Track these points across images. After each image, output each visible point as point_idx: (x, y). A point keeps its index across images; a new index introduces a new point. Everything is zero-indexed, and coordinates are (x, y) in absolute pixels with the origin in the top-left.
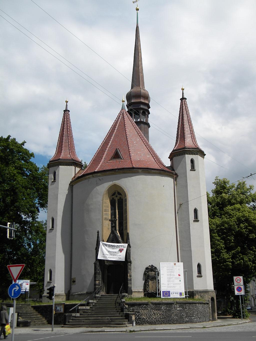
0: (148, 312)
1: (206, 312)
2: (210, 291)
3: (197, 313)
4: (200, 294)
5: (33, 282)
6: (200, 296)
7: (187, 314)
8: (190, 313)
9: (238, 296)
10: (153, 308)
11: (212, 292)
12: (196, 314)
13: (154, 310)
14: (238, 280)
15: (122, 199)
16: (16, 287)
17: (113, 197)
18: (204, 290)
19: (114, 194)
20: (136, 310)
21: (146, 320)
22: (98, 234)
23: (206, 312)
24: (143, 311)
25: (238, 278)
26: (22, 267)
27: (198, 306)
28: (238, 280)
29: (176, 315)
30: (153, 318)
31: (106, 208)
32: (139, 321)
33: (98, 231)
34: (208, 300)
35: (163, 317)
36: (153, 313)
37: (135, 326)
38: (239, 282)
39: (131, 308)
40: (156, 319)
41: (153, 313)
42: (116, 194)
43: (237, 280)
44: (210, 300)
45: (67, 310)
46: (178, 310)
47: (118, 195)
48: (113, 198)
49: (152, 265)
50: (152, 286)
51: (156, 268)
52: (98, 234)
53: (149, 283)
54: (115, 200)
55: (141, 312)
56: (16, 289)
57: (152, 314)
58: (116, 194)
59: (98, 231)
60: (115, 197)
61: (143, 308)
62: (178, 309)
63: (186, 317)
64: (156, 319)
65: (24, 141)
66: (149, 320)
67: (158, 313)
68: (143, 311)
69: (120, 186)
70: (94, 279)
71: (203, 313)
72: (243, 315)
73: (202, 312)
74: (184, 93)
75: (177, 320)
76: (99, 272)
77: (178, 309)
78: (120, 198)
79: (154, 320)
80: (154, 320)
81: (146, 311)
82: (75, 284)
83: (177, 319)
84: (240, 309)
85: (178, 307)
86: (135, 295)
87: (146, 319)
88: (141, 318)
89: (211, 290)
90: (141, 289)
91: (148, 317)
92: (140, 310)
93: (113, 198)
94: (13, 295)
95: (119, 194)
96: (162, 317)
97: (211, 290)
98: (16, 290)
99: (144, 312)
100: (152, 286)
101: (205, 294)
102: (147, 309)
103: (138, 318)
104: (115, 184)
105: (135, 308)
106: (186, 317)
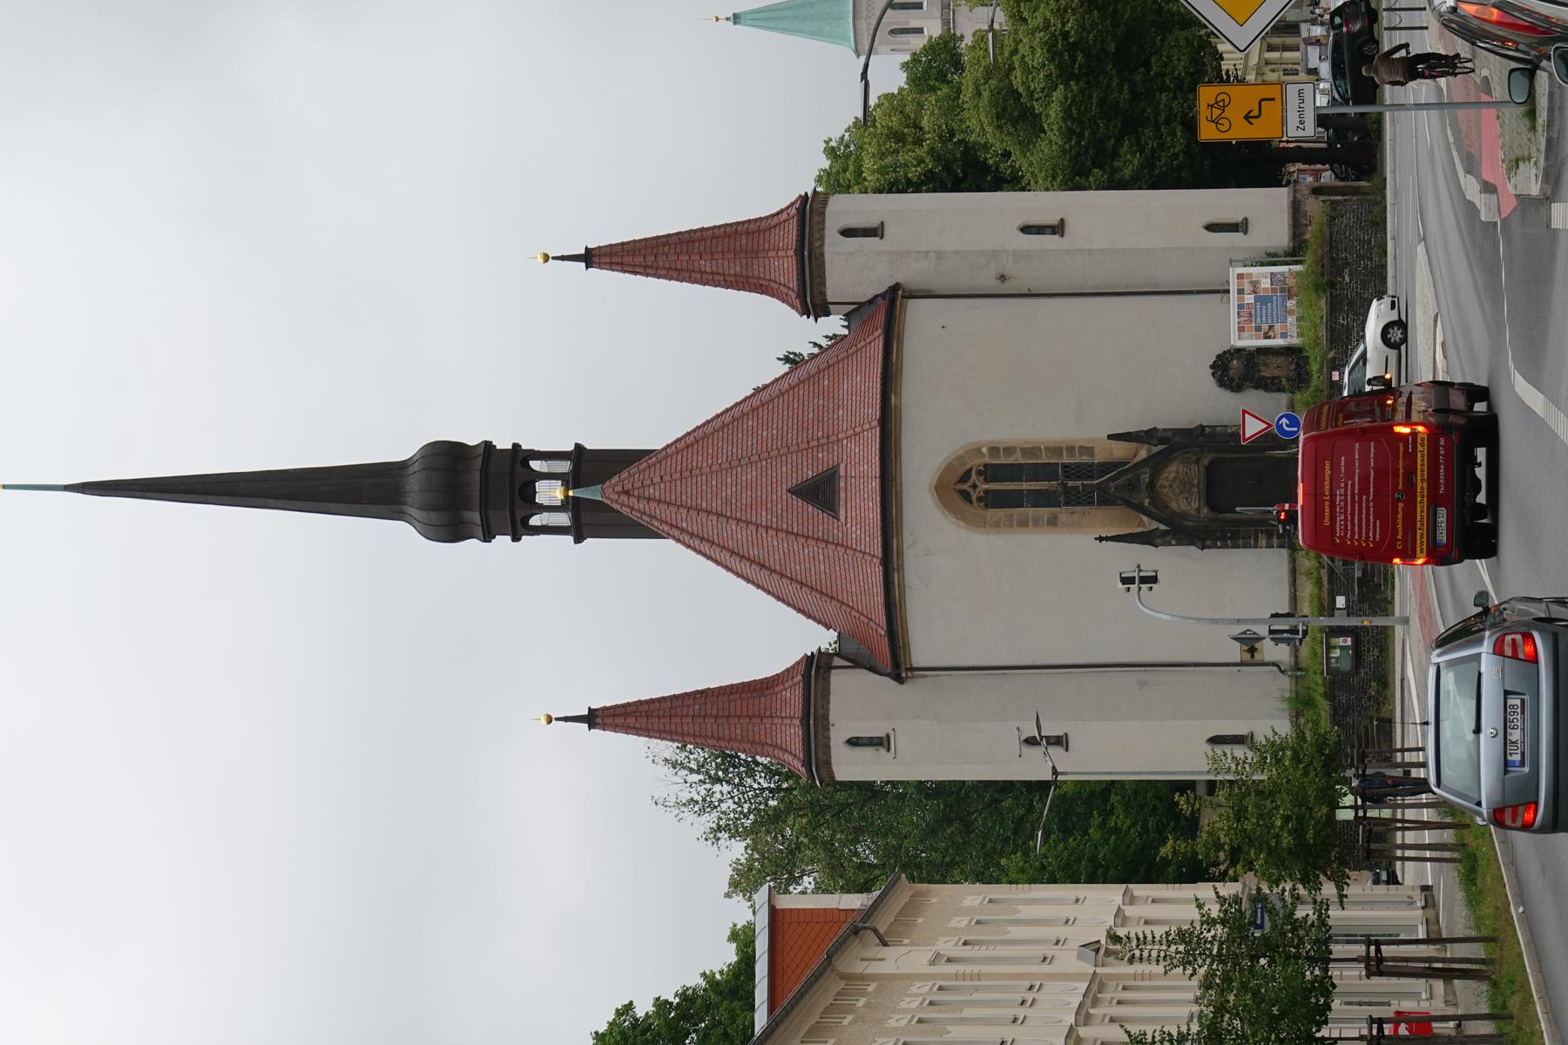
1: (1358, 208)
2: (1294, 197)
7: (1361, 257)
10: (1342, 347)
11: (1295, 191)
15: (986, 466)
16: (1282, 424)
17: (974, 497)
19: (965, 496)
26: (1247, 437)
29: (1364, 286)
31: (1015, 523)
34: (1321, 204)
42: (965, 487)
44: (1321, 198)
47: (970, 483)
48: (980, 499)
49: (1212, 367)
52: (1107, 539)
53: (1269, 375)
54: (986, 492)
56: (1286, 425)
58: (965, 487)
59: (1096, 539)
63: (1370, 259)
67: (1358, 334)
69: (942, 468)
71: (1362, 213)
74: (560, 255)
77: (1347, 279)
78: (979, 473)
84: (924, 175)
89: (1288, 193)
90: (1284, 398)
93: (980, 499)
94: (1296, 429)
95: (965, 477)
97: (1288, 196)
98: (1288, 422)
100: (1275, 368)
104: (935, 487)
106: (1370, 259)
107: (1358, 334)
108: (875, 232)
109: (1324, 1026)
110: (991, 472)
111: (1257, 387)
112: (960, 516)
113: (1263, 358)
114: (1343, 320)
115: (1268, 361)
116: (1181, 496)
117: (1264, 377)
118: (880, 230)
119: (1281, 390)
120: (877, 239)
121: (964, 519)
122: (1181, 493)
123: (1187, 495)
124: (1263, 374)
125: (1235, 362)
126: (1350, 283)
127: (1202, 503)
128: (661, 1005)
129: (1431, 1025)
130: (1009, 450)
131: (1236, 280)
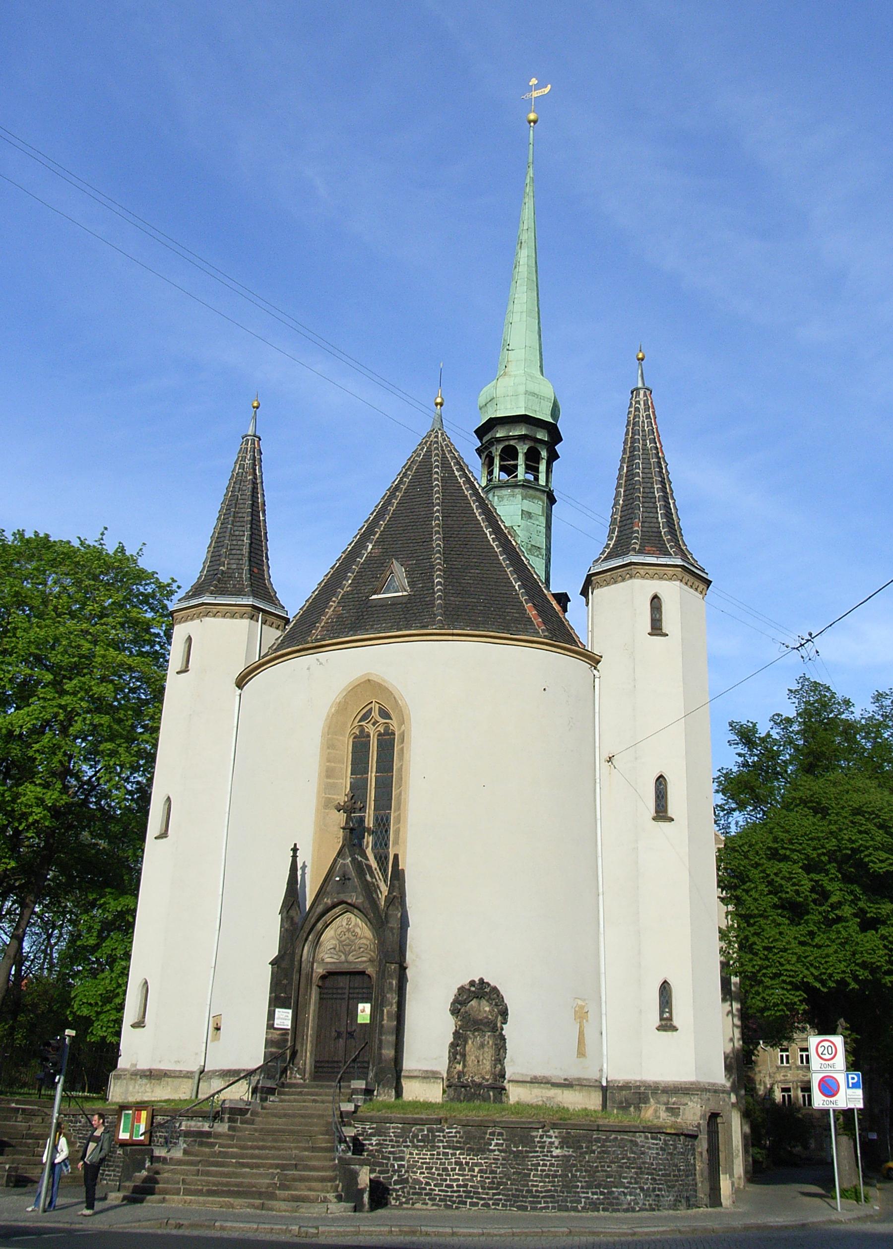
0: (437, 1159)
3: (636, 1173)
4: (664, 1098)
5: (725, 1062)
6: (664, 1107)
7: (592, 1172)
8: (606, 1171)
9: (826, 1112)
10: (458, 1142)
12: (631, 1178)
13: (458, 1152)
14: (826, 1052)
18: (681, 1083)
20: (393, 1147)
21: (428, 1187)
22: (295, 857)
23: (679, 1170)
24: (416, 1154)
25: (826, 1044)
27: (643, 1146)
28: (826, 1052)
30: (455, 1184)
31: (333, 764)
32: (400, 1193)
33: (295, 845)
35: (493, 1182)
36: (456, 1163)
37: (367, 1212)
38: (827, 1057)
39: (374, 1138)
40: (466, 1186)
41: (456, 1163)
43: (820, 1050)
45: (158, 1134)
46: (557, 1156)
49: (481, 980)
50: (476, 1057)
51: (495, 990)
52: (295, 857)
53: (467, 1048)
54: (369, 736)
55: (408, 1156)
57: (449, 1167)
59: (295, 845)
60: (370, 725)
61: (419, 1141)
62: (557, 1152)
64: (466, 1186)
65: (23, 530)
66: (447, 1192)
67: (476, 1165)
68: (416, 1154)
70: (268, 1020)
72: (866, 1198)
73: (660, 1170)
75: (552, 1197)
76: (285, 997)
77: (557, 1152)
79: (459, 1191)
80: (459, 1191)
81: (427, 1155)
82: (219, 1039)
83: (550, 1191)
85: (556, 1144)
86: (413, 1091)
87: (428, 1184)
88: (406, 1181)
90: (442, 1066)
91: (433, 1179)
92: (405, 1146)
95: (385, 714)
96: (489, 1183)
99: (421, 1156)
101: (685, 1099)
102: (434, 1147)
103: (395, 1178)
105: (386, 1140)
107: (476, 1165)
108: (657, 629)
109: (577, 1109)
110: (387, 742)
111: (456, 1034)
112: (342, 708)
113: (491, 1043)
114: (497, 1144)
115: (486, 1049)
116: (337, 942)
117: (466, 1042)
118: (659, 632)
119: (453, 1059)
120: (649, 630)
121: (338, 712)
122: (341, 942)
123: (337, 949)
124: (470, 1042)
125: (487, 1009)
126: (552, 1156)
127: (329, 966)
128: (20, 534)
129: (867, 1098)
130: (401, 758)
131: (367, 815)
